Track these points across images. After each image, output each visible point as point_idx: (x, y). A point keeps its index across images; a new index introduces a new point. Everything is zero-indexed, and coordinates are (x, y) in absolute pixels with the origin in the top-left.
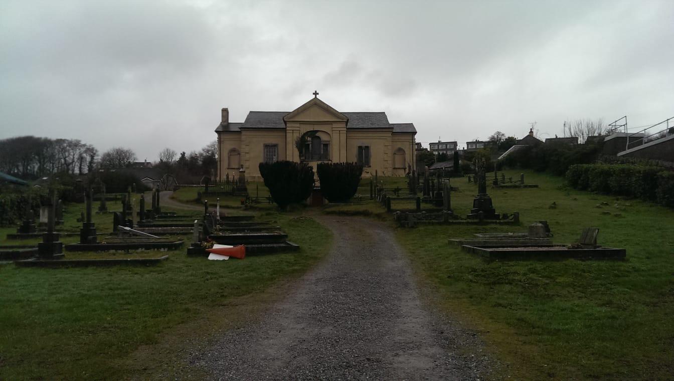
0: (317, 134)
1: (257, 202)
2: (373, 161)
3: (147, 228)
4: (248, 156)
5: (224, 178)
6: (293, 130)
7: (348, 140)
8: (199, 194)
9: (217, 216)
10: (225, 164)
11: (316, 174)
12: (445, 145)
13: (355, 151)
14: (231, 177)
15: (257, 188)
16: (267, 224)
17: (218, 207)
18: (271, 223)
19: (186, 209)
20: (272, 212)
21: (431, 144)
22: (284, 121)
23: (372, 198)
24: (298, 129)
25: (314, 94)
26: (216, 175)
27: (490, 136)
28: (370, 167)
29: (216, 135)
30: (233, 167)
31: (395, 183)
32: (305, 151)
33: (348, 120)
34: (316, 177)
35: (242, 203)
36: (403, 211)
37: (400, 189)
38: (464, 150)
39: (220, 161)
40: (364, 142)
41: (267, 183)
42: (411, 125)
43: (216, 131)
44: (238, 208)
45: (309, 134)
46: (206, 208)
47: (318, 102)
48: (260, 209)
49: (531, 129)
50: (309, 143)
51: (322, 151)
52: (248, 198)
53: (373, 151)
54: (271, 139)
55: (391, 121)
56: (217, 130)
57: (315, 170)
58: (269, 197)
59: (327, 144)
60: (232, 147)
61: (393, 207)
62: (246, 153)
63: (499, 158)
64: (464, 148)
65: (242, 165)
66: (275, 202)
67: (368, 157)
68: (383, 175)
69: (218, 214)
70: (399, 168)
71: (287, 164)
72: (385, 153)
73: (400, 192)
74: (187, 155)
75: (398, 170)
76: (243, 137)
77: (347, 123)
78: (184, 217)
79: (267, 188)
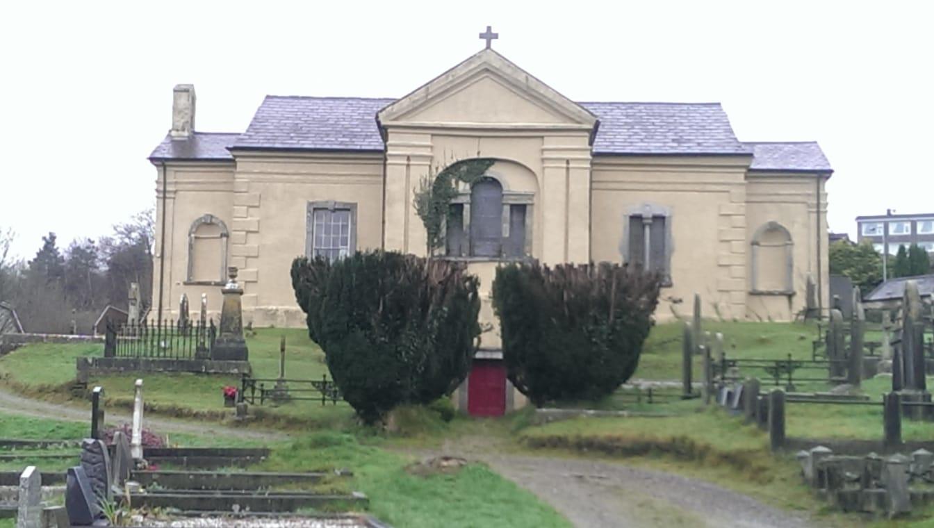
0: (492, 172)
1: (280, 396)
3: (234, 362)
4: (253, 241)
5: (172, 313)
6: (408, 158)
7: (593, 192)
8: (83, 364)
9: (134, 446)
10: (178, 268)
12: (908, 225)
14: (194, 313)
15: (283, 350)
16: (315, 480)
17: (137, 413)
18: (328, 476)
19: (30, 415)
20: (334, 435)
21: (861, 220)
22: (378, 123)
23: (689, 394)
25: (482, 36)
26: (145, 306)
29: (153, 172)
31: (762, 342)
32: (448, 228)
33: (597, 124)
34: (488, 316)
35: (230, 398)
36: (840, 447)
39: (162, 256)
40: (649, 202)
41: (317, 333)
43: (152, 159)
44: (213, 417)
45: (464, 168)
46: (97, 416)
47: (497, 64)
48: (292, 423)
51: (506, 227)
52: (248, 381)
53: (679, 232)
56: (158, 155)
57: (484, 292)
58: (325, 383)
59: (524, 206)
60: (203, 212)
61: (794, 428)
62: (248, 232)
65: (234, 270)
66: (346, 399)
67: (661, 250)
68: (715, 316)
69: (137, 439)
70: (770, 294)
71: (394, 261)
72: (722, 241)
73: (797, 373)
74: (63, 247)
76: (241, 179)
77: (593, 133)
78: (20, 444)
79: (320, 352)
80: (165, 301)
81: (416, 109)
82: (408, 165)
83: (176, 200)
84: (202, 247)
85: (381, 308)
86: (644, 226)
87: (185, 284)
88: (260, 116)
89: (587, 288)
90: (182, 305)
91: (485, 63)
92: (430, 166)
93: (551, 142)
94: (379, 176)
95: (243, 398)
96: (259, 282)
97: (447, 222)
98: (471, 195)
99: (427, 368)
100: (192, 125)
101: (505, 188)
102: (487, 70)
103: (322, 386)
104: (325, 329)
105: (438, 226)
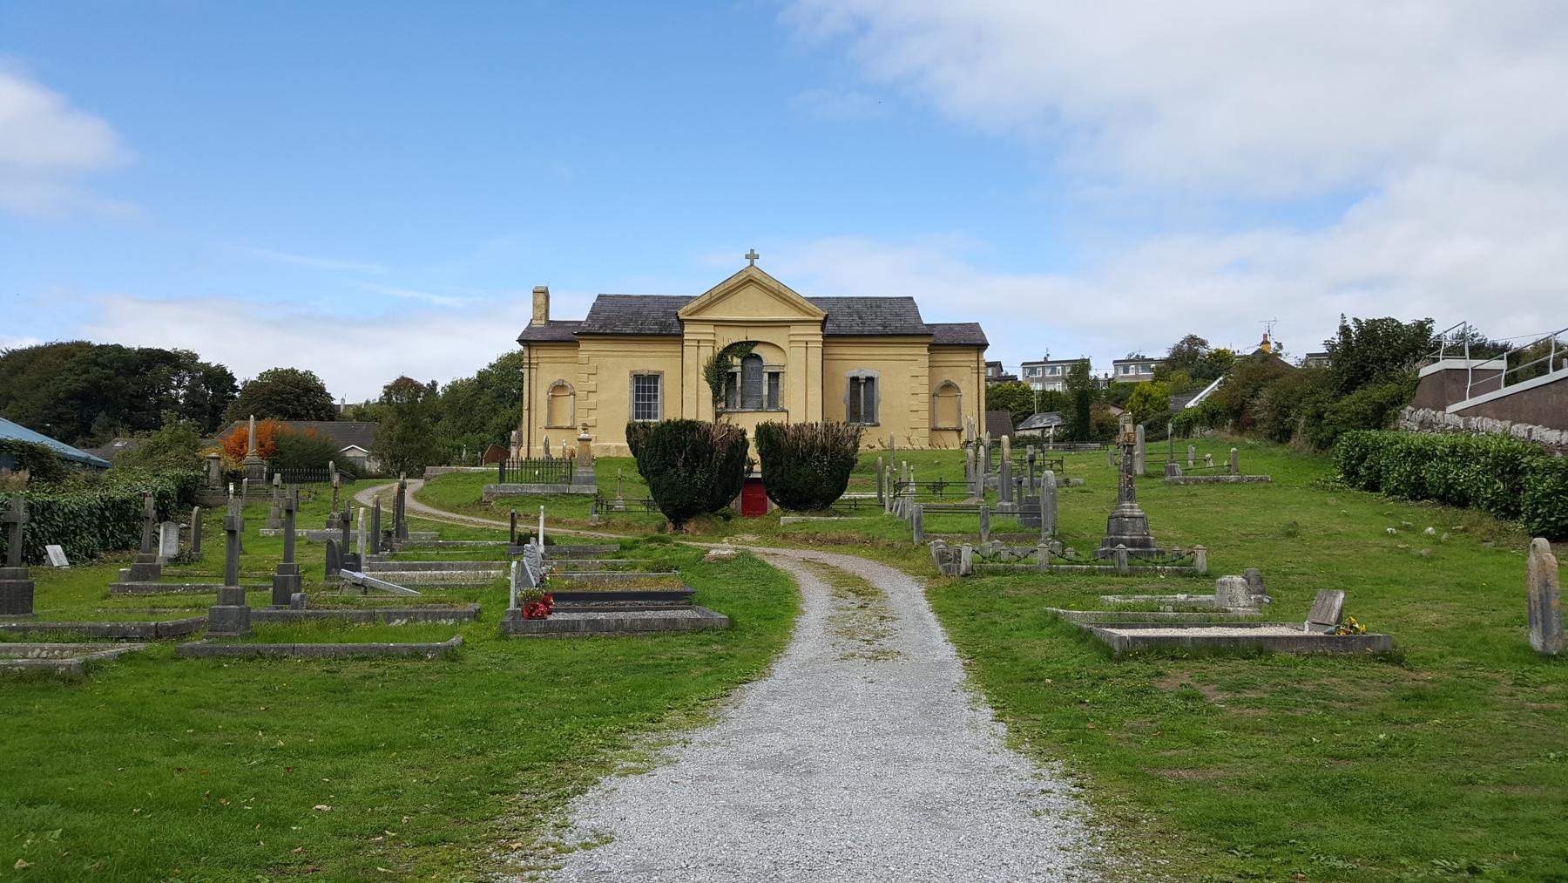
0: (755, 351)
4: (593, 399)
6: (699, 341)
11: (752, 444)
13: (843, 389)
24: (711, 337)
27: (1172, 346)
28: (878, 425)
32: (726, 390)
34: (753, 453)
37: (948, 484)
38: (1109, 382)
42: (974, 328)
47: (758, 276)
49: (1265, 336)
53: (882, 388)
54: (648, 359)
55: (927, 319)
56: (524, 338)
57: (751, 435)
60: (556, 378)
62: (589, 392)
63: (1190, 404)
64: (1106, 375)
71: (691, 426)
75: (943, 433)
80: (532, 440)
82: (698, 347)
83: (538, 370)
85: (684, 455)
86: (860, 384)
87: (546, 428)
88: (595, 310)
89: (814, 438)
90: (545, 443)
91: (750, 275)
92: (714, 347)
93: (794, 330)
94: (678, 352)
96: (598, 426)
97: (726, 385)
98: (742, 367)
101: (765, 361)
103: (647, 503)
104: (649, 469)
105: (719, 388)
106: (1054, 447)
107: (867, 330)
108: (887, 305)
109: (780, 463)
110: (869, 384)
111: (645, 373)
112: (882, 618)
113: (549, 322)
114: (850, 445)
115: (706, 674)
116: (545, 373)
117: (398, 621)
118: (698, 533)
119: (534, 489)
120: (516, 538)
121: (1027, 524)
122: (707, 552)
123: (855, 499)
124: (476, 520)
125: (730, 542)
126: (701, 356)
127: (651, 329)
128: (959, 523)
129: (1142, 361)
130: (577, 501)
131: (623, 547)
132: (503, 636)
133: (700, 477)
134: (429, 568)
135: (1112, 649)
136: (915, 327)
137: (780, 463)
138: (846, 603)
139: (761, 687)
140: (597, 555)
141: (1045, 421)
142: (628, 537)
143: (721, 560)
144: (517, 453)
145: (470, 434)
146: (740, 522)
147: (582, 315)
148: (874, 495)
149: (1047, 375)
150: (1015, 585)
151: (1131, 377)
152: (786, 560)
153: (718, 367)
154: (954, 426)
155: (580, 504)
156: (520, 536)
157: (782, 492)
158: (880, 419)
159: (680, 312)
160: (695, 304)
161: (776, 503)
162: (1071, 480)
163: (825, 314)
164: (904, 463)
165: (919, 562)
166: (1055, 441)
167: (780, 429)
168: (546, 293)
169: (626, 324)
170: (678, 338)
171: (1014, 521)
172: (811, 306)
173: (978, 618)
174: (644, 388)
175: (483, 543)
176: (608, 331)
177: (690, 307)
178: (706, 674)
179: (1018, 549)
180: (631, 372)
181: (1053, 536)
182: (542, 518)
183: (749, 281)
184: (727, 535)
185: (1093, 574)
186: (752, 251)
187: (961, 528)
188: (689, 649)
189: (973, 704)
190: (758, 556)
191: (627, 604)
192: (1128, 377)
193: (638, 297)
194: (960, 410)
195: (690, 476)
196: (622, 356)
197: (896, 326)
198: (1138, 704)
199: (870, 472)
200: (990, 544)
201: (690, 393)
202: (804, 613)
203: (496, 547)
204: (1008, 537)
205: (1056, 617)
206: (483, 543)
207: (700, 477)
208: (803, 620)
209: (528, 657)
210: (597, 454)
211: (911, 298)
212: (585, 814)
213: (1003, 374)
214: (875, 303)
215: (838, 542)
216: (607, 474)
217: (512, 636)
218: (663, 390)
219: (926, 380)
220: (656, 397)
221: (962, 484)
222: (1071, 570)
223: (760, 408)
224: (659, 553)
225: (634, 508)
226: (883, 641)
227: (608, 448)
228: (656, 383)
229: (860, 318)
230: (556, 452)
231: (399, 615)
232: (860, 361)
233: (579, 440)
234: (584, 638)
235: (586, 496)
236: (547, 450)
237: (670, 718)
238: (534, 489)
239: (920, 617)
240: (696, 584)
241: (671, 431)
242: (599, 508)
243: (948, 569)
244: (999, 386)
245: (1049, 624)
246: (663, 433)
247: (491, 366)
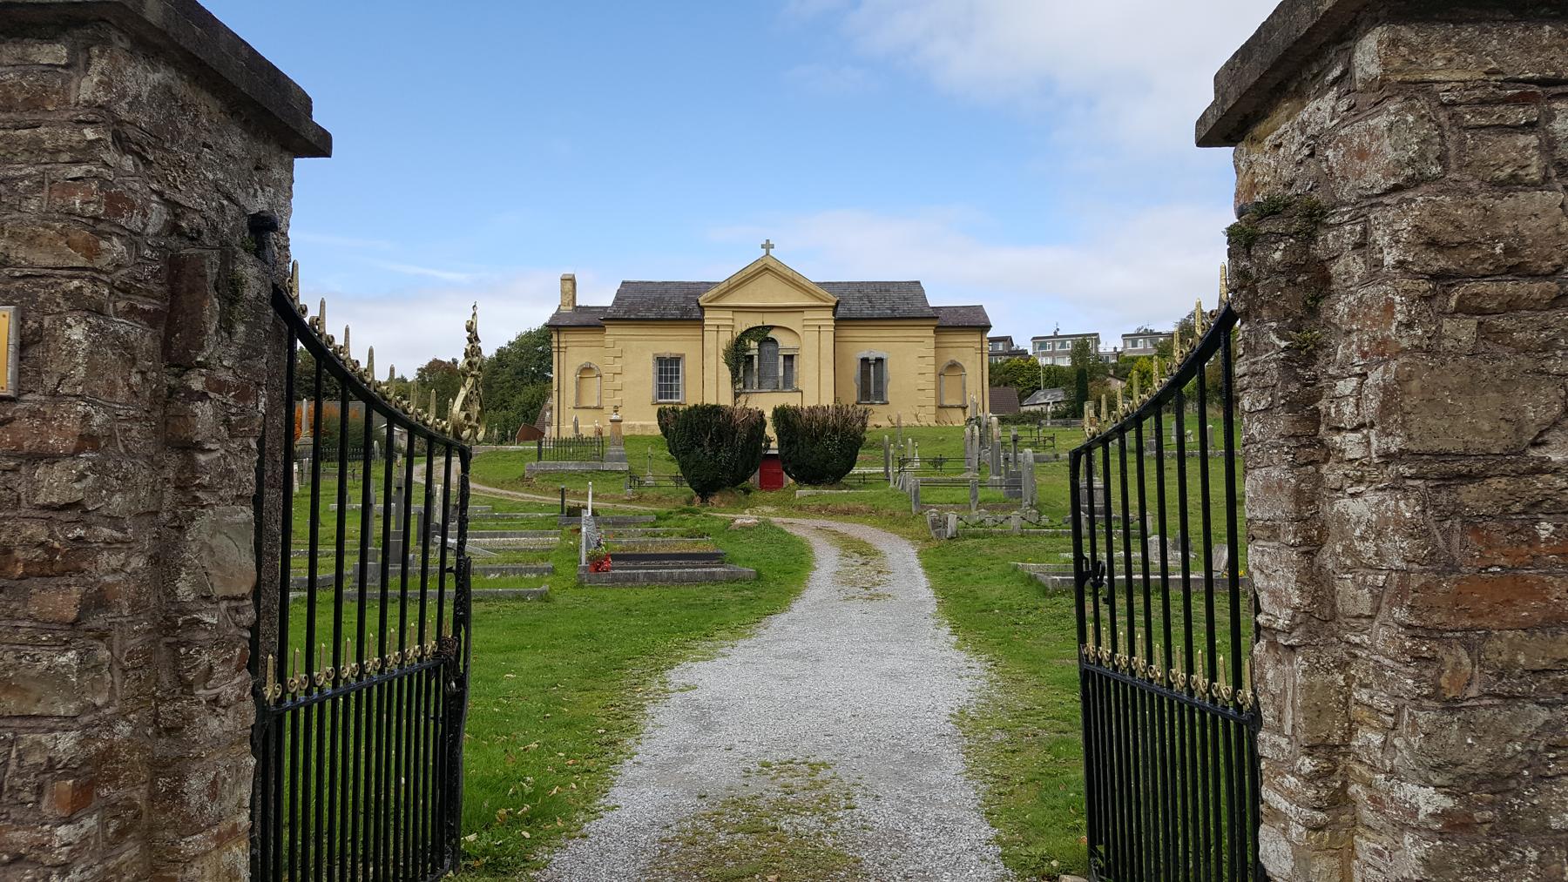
0: (771, 334)
2: (891, 390)
4: (619, 380)
6: (718, 326)
13: (854, 370)
24: (730, 323)
25: (763, 247)
27: (1179, 321)
28: (887, 403)
30: (587, 405)
34: (770, 431)
37: (947, 460)
38: (1118, 355)
42: (978, 310)
47: (773, 264)
50: (751, 353)
53: (891, 368)
54: (670, 342)
55: (933, 301)
56: (553, 323)
60: (583, 361)
64: (1115, 348)
67: (880, 382)
71: (716, 410)
75: (948, 410)
80: (562, 420)
81: (722, 295)
84: (586, 382)
89: (826, 420)
93: (808, 315)
95: (1365, 671)
99: (736, 467)
100: (574, 302)
101: (780, 345)
102: (767, 269)
103: (676, 479)
104: (679, 448)
105: (738, 370)
106: (1052, 424)
107: (876, 313)
108: (896, 289)
109: (795, 442)
110: (879, 364)
111: (668, 356)
112: (879, 572)
113: (576, 308)
114: (859, 424)
115: (741, 610)
116: (86, 55)
117: (492, 575)
118: (723, 505)
119: (572, 466)
120: (566, 511)
121: (1011, 495)
122: (733, 520)
123: (864, 474)
124: (520, 495)
125: (751, 513)
126: (720, 340)
127: (672, 314)
128: (953, 495)
129: (1149, 335)
130: (610, 477)
131: (659, 518)
132: (580, 585)
133: (724, 455)
134: (495, 536)
135: (1047, 589)
136: (922, 311)
137: (795, 442)
138: (851, 561)
139: (784, 617)
140: (637, 525)
141: (1049, 397)
142: (663, 509)
143: (745, 528)
144: (550, 432)
145: (492, 412)
146: (758, 495)
147: (608, 301)
148: (881, 470)
149: (1057, 349)
150: (991, 546)
151: (1140, 351)
152: (801, 528)
153: (737, 350)
154: (959, 403)
155: (614, 480)
156: (569, 509)
157: (797, 468)
158: (889, 397)
159: (700, 299)
160: (714, 291)
161: (792, 478)
162: (1061, 456)
163: (836, 300)
164: (910, 440)
165: (916, 528)
166: (1052, 418)
167: (796, 412)
168: (572, 280)
169: (649, 310)
170: (699, 322)
171: (1000, 493)
172: (823, 292)
173: (956, 571)
174: (666, 370)
175: (534, 515)
176: (632, 317)
177: (710, 294)
178: (741, 610)
179: (1000, 516)
180: (654, 355)
181: (1031, 505)
182: (590, 493)
183: (764, 269)
184: (748, 507)
185: (1057, 536)
186: (768, 241)
187: (953, 499)
188: (726, 594)
189: (938, 626)
190: (777, 525)
191: (671, 563)
192: (1135, 351)
193: (659, 283)
194: (964, 388)
195: (716, 455)
196: (646, 340)
197: (903, 309)
198: (1056, 624)
199: (879, 448)
200: (977, 513)
201: (710, 375)
202: (816, 569)
203: (547, 518)
204: (993, 506)
205: (1016, 569)
206: (534, 515)
207: (724, 455)
208: (816, 574)
209: (603, 599)
210: (625, 432)
211: (918, 283)
212: (675, 677)
213: (1014, 348)
214: (884, 288)
215: (847, 513)
216: (635, 452)
217: (586, 585)
218: (684, 371)
219: (932, 360)
220: (678, 378)
221: (962, 459)
222: (1039, 533)
223: (776, 389)
224: (690, 523)
225: (661, 483)
226: (877, 588)
227: (633, 427)
228: (678, 365)
229: (870, 302)
230: (587, 430)
231: (493, 570)
232: (870, 344)
233: (611, 421)
234: (642, 587)
235: (619, 472)
236: (577, 429)
237: (718, 635)
238: (572, 466)
239: (910, 571)
240: (726, 547)
241: (698, 414)
242: (632, 484)
243: (938, 534)
244: (1008, 361)
245: (1009, 574)
246: (691, 416)
247: (510, 344)
